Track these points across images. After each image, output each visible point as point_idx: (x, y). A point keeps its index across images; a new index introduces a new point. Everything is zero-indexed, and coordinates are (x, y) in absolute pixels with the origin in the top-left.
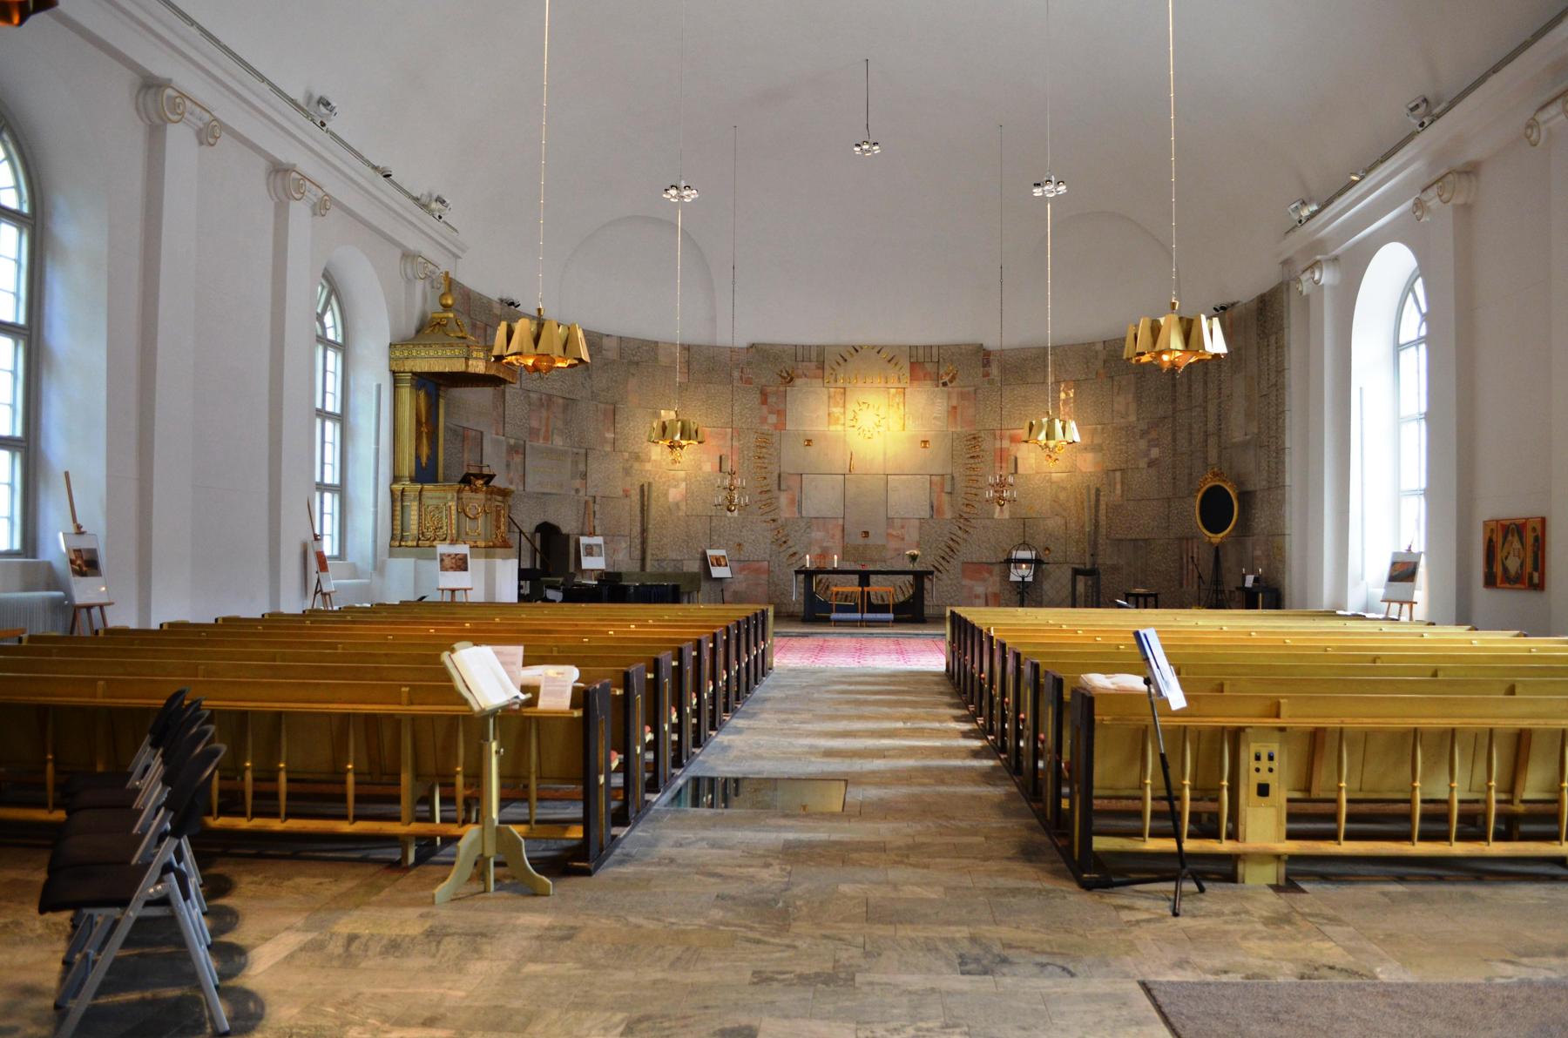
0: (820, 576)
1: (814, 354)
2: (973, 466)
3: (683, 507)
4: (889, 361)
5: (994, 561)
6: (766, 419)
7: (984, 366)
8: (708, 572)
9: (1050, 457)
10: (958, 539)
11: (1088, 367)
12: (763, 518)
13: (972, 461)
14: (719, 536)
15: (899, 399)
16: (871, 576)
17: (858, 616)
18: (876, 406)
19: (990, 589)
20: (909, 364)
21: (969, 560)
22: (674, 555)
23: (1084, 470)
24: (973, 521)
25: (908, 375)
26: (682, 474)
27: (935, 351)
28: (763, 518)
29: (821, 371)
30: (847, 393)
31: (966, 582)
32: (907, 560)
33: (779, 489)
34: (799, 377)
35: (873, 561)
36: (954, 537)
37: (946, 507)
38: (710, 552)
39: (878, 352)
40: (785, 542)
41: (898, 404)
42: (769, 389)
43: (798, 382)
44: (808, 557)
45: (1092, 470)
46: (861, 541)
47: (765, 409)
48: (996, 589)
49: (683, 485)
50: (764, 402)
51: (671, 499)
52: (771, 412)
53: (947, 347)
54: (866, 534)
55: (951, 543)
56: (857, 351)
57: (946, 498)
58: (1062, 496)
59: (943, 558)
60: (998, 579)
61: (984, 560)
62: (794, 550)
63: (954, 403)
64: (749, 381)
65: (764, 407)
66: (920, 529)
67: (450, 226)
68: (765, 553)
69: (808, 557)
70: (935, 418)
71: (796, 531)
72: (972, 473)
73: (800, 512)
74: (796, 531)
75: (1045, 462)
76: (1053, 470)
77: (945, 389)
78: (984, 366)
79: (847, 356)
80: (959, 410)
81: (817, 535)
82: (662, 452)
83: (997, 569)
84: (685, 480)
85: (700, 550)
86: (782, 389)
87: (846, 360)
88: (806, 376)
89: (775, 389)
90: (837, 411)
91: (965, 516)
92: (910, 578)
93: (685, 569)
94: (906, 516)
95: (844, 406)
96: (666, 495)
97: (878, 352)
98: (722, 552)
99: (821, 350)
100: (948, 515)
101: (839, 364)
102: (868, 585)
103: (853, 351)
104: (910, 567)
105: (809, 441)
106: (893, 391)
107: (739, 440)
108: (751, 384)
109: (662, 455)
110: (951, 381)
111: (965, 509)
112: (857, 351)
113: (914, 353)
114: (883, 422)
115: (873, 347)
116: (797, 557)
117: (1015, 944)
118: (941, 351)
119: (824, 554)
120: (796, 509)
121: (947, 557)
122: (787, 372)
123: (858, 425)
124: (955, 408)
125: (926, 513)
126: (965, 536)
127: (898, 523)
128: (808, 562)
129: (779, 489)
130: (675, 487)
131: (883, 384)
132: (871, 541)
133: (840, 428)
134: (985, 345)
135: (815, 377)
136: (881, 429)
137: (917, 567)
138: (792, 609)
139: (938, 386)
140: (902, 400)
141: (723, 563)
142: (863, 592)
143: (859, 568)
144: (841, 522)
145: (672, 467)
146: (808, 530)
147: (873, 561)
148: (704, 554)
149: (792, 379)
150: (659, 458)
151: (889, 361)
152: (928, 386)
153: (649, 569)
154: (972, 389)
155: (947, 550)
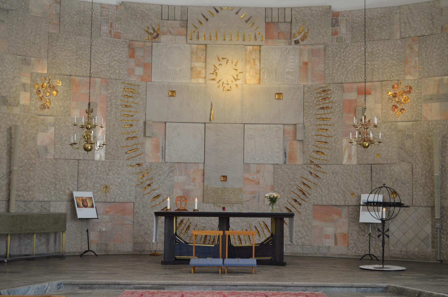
0: (180, 219)
1: (178, 15)
2: (323, 116)
3: (51, 150)
4: (247, 21)
5: (343, 203)
6: (133, 71)
7: (333, 26)
8: (74, 213)
9: (396, 107)
10: (309, 184)
11: (433, 23)
12: (129, 162)
13: (322, 112)
14: (86, 178)
15: (255, 55)
16: (232, 219)
17: (219, 261)
18: (235, 62)
19: (339, 231)
20: (264, 23)
21: (320, 203)
22: (41, 197)
23: (429, 118)
24: (322, 167)
25: (264, 34)
26: (51, 119)
27: (288, 13)
28: (129, 162)
29: (184, 29)
30: (208, 49)
31: (316, 223)
32: (268, 202)
33: (145, 135)
34: (164, 34)
35: (232, 204)
36: (305, 182)
37: (298, 154)
38: (76, 194)
39: (237, 13)
40: (149, 185)
41: (254, 60)
42: (136, 44)
43: (163, 38)
44: (169, 199)
45: (437, 118)
46: (220, 184)
47: (132, 62)
48: (344, 229)
49: (52, 130)
50: (132, 56)
51: (39, 143)
52: (138, 65)
53: (300, 9)
54: (225, 178)
55: (302, 186)
56: (217, 11)
57: (297, 146)
58: (408, 143)
59: (295, 201)
60: (346, 220)
61: (334, 203)
62: (157, 192)
63: (306, 60)
64: (117, 36)
65: (132, 60)
66: (274, 173)
67: (192, 163)
68: (130, 195)
69: (169, 199)
70: (288, 73)
71: (160, 175)
72: (322, 122)
73: (164, 157)
74: (160, 175)
75: (391, 112)
76: (399, 119)
77: (298, 46)
78: (333, 26)
79: (208, 16)
80: (310, 66)
81: (180, 178)
82: (31, 97)
83: (345, 211)
84: (54, 125)
85: (67, 192)
86: (149, 44)
87: (207, 20)
88: (170, 33)
89: (141, 44)
90: (199, 65)
91: (316, 162)
92: (268, 221)
93: (52, 210)
94: (261, 161)
95: (206, 62)
96: (34, 139)
97: (237, 13)
98: (89, 194)
99: (185, 10)
100: (300, 161)
101: (201, 23)
102: (228, 228)
103: (214, 12)
104: (269, 210)
105: (173, 92)
106: (250, 48)
107: (107, 89)
108: (120, 38)
109: (31, 99)
110: (303, 40)
111: (315, 155)
112: (217, 11)
113: (269, 14)
114: (240, 76)
115: (232, 8)
116: (160, 199)
117: (256, 285)
118: (294, 12)
119: (184, 198)
120: (160, 154)
121: (299, 200)
122: (154, 29)
123: (218, 79)
124: (306, 64)
125: (280, 159)
126: (316, 181)
127: (253, 168)
128: (169, 205)
129: (145, 135)
130: (44, 131)
131: (240, 42)
132: (229, 184)
133: (201, 81)
134: (333, 8)
135: (179, 34)
136: (238, 82)
137: (277, 209)
138: (155, 248)
139: (290, 44)
140: (258, 56)
141: (89, 204)
142: (224, 236)
143: (220, 210)
144: (201, 167)
145: (42, 112)
146: (171, 174)
147: (232, 204)
148: (72, 195)
149: (158, 35)
150: (28, 103)
151: (247, 21)
152: (282, 44)
153: (13, 210)
154: (322, 47)
155: (300, 193)
